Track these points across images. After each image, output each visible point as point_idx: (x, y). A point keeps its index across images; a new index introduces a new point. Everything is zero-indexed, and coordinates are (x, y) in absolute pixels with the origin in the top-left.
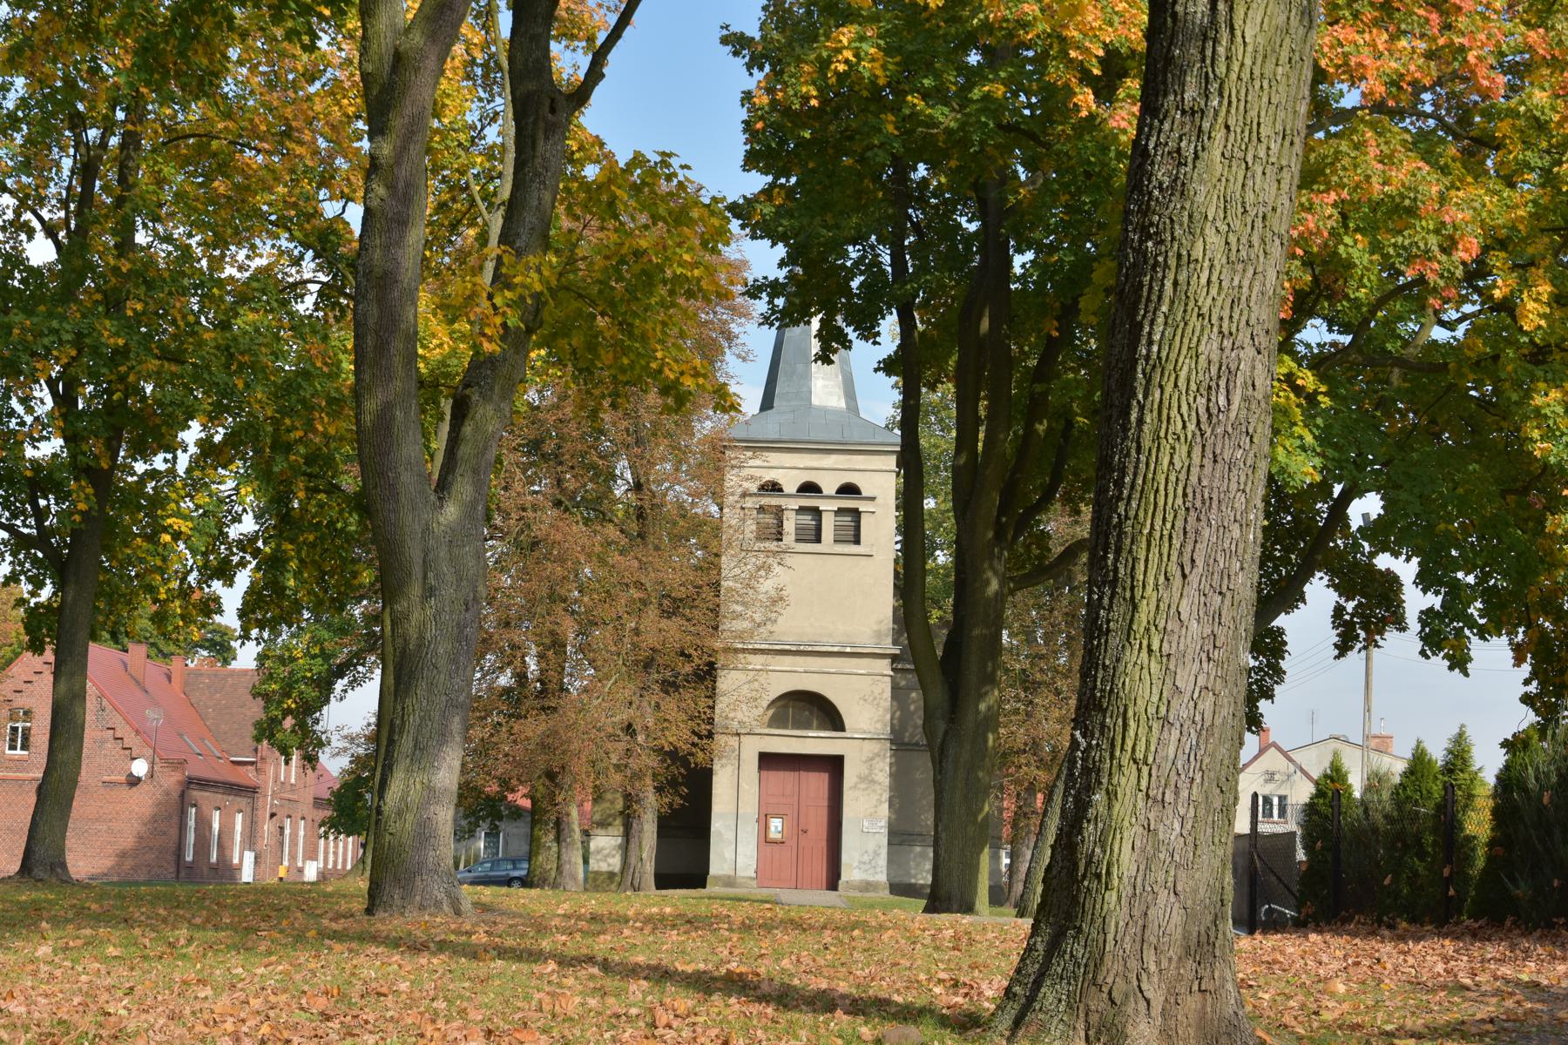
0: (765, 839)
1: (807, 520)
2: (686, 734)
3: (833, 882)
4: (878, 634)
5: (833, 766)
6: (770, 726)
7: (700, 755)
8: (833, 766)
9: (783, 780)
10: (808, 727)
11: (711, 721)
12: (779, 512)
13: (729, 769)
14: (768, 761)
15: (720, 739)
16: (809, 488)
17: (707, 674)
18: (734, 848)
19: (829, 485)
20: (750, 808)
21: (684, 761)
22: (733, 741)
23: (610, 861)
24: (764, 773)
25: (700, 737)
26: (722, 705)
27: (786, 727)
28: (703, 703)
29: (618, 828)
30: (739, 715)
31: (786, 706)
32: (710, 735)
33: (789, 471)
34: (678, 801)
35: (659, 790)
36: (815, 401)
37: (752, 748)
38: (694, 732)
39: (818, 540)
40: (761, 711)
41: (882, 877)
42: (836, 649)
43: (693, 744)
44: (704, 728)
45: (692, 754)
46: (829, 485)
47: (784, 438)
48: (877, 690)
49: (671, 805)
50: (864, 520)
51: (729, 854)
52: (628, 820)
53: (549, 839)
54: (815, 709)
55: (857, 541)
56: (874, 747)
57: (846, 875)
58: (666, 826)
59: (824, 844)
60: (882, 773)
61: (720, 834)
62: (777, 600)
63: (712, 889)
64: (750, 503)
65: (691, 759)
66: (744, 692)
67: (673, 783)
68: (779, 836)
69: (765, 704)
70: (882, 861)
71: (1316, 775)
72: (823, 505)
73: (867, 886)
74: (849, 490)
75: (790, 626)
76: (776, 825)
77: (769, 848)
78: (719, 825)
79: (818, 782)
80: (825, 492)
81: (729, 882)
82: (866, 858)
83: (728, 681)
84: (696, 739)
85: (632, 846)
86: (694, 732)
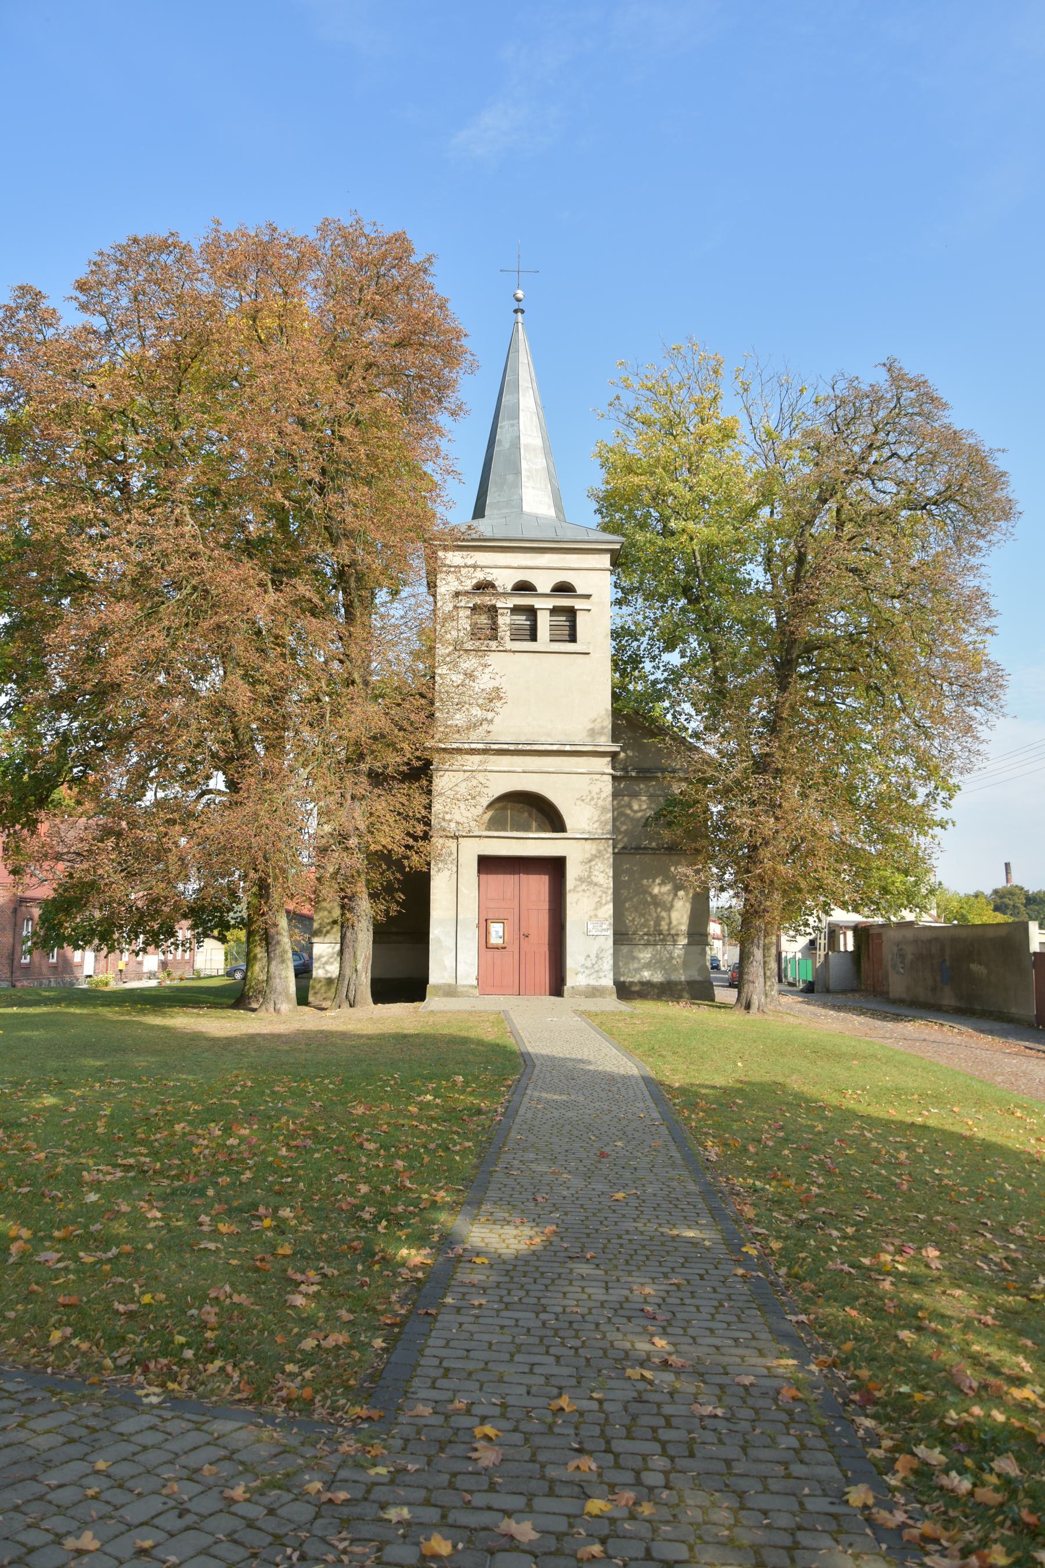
0: (486, 945)
1: (522, 620)
2: (399, 835)
3: (557, 986)
4: (592, 733)
5: (554, 868)
6: (489, 829)
7: (415, 857)
8: (554, 868)
9: (503, 883)
10: (527, 829)
11: (428, 824)
12: (493, 611)
13: (447, 873)
14: (488, 864)
15: (437, 841)
16: (524, 587)
17: (420, 773)
18: (454, 952)
19: (544, 583)
20: (470, 913)
21: (398, 865)
22: (452, 844)
23: (328, 967)
24: (483, 877)
25: (416, 839)
26: (437, 807)
27: (505, 830)
28: (419, 800)
29: (335, 934)
30: (457, 817)
31: (504, 808)
32: (426, 837)
33: (504, 570)
34: (394, 907)
35: (373, 896)
36: (526, 508)
37: (471, 851)
38: (408, 834)
39: (533, 638)
40: (480, 810)
41: (608, 981)
42: (555, 748)
43: (407, 847)
44: (420, 829)
45: (408, 858)
46: (544, 583)
47: (497, 536)
48: (595, 789)
49: (387, 912)
50: (581, 619)
51: (449, 962)
52: (344, 926)
53: (259, 951)
54: (537, 810)
55: (573, 639)
56: (591, 848)
57: (573, 980)
58: (381, 933)
59: (546, 948)
60: (604, 875)
61: (439, 941)
62: (495, 696)
63: (433, 1002)
64: (463, 601)
65: (406, 862)
66: (460, 796)
67: (389, 889)
68: (501, 941)
69: (485, 802)
70: (608, 963)
71: (1017, 880)
72: (537, 603)
73: (594, 992)
74: (563, 589)
75: (508, 725)
76: (496, 930)
77: (490, 953)
78: (439, 931)
79: (539, 885)
80: (540, 591)
81: (450, 991)
82: (589, 964)
83: (446, 781)
84: (411, 842)
85: (346, 956)
86: (408, 834)
